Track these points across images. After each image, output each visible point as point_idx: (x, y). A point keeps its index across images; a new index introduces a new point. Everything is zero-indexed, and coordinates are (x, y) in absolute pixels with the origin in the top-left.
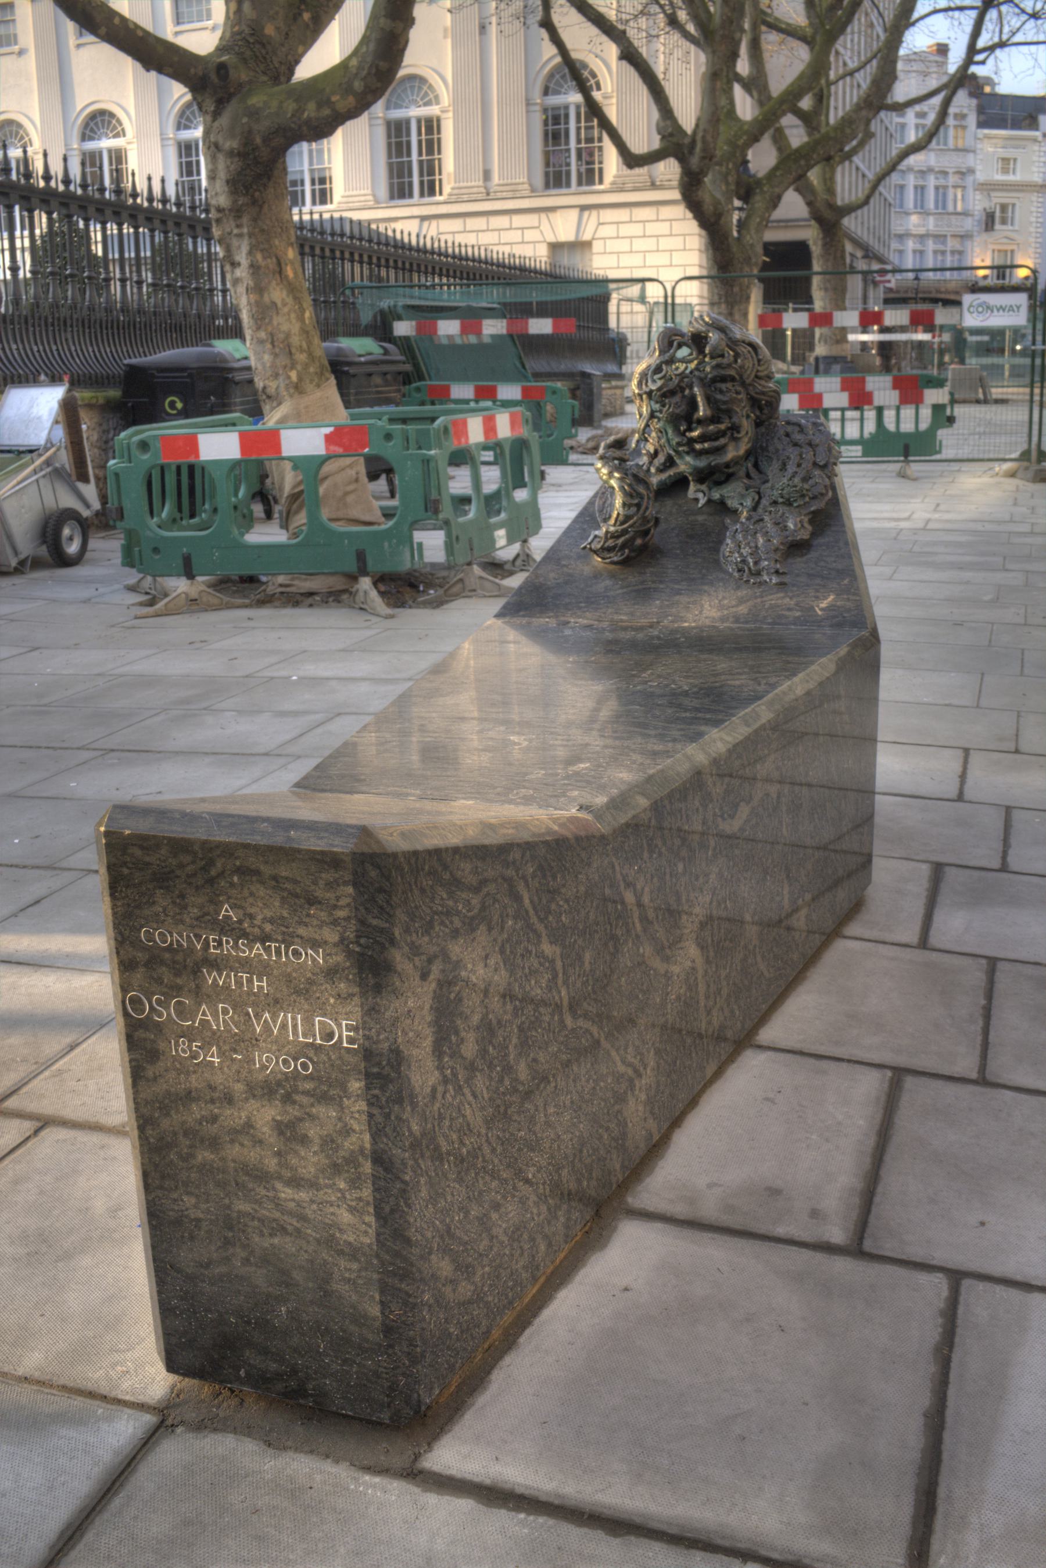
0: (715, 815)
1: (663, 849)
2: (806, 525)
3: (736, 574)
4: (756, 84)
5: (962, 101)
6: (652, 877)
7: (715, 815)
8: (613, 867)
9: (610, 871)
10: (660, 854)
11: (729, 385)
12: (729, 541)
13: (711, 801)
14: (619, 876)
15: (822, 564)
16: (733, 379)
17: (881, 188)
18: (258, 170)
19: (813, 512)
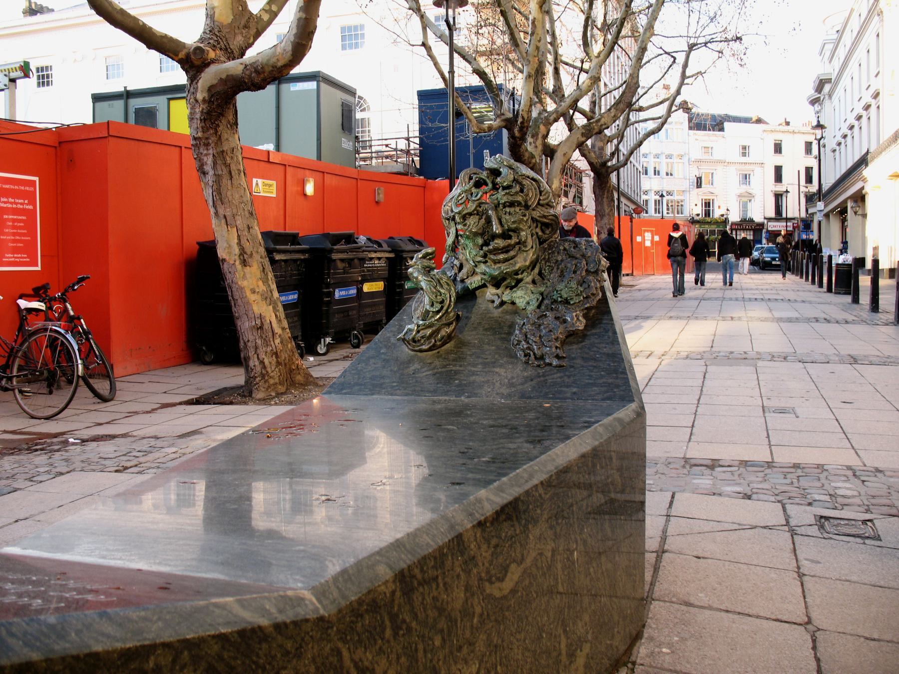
0: (481, 579)
1: (414, 624)
2: (581, 318)
3: (524, 359)
4: (557, 94)
5: (680, 117)
6: (398, 658)
7: (481, 579)
8: (339, 653)
9: (334, 660)
10: (409, 630)
11: (517, 209)
12: (517, 332)
13: (476, 565)
14: (347, 663)
15: (595, 349)
16: (519, 204)
17: (631, 159)
18: (218, 109)
19: (586, 308)
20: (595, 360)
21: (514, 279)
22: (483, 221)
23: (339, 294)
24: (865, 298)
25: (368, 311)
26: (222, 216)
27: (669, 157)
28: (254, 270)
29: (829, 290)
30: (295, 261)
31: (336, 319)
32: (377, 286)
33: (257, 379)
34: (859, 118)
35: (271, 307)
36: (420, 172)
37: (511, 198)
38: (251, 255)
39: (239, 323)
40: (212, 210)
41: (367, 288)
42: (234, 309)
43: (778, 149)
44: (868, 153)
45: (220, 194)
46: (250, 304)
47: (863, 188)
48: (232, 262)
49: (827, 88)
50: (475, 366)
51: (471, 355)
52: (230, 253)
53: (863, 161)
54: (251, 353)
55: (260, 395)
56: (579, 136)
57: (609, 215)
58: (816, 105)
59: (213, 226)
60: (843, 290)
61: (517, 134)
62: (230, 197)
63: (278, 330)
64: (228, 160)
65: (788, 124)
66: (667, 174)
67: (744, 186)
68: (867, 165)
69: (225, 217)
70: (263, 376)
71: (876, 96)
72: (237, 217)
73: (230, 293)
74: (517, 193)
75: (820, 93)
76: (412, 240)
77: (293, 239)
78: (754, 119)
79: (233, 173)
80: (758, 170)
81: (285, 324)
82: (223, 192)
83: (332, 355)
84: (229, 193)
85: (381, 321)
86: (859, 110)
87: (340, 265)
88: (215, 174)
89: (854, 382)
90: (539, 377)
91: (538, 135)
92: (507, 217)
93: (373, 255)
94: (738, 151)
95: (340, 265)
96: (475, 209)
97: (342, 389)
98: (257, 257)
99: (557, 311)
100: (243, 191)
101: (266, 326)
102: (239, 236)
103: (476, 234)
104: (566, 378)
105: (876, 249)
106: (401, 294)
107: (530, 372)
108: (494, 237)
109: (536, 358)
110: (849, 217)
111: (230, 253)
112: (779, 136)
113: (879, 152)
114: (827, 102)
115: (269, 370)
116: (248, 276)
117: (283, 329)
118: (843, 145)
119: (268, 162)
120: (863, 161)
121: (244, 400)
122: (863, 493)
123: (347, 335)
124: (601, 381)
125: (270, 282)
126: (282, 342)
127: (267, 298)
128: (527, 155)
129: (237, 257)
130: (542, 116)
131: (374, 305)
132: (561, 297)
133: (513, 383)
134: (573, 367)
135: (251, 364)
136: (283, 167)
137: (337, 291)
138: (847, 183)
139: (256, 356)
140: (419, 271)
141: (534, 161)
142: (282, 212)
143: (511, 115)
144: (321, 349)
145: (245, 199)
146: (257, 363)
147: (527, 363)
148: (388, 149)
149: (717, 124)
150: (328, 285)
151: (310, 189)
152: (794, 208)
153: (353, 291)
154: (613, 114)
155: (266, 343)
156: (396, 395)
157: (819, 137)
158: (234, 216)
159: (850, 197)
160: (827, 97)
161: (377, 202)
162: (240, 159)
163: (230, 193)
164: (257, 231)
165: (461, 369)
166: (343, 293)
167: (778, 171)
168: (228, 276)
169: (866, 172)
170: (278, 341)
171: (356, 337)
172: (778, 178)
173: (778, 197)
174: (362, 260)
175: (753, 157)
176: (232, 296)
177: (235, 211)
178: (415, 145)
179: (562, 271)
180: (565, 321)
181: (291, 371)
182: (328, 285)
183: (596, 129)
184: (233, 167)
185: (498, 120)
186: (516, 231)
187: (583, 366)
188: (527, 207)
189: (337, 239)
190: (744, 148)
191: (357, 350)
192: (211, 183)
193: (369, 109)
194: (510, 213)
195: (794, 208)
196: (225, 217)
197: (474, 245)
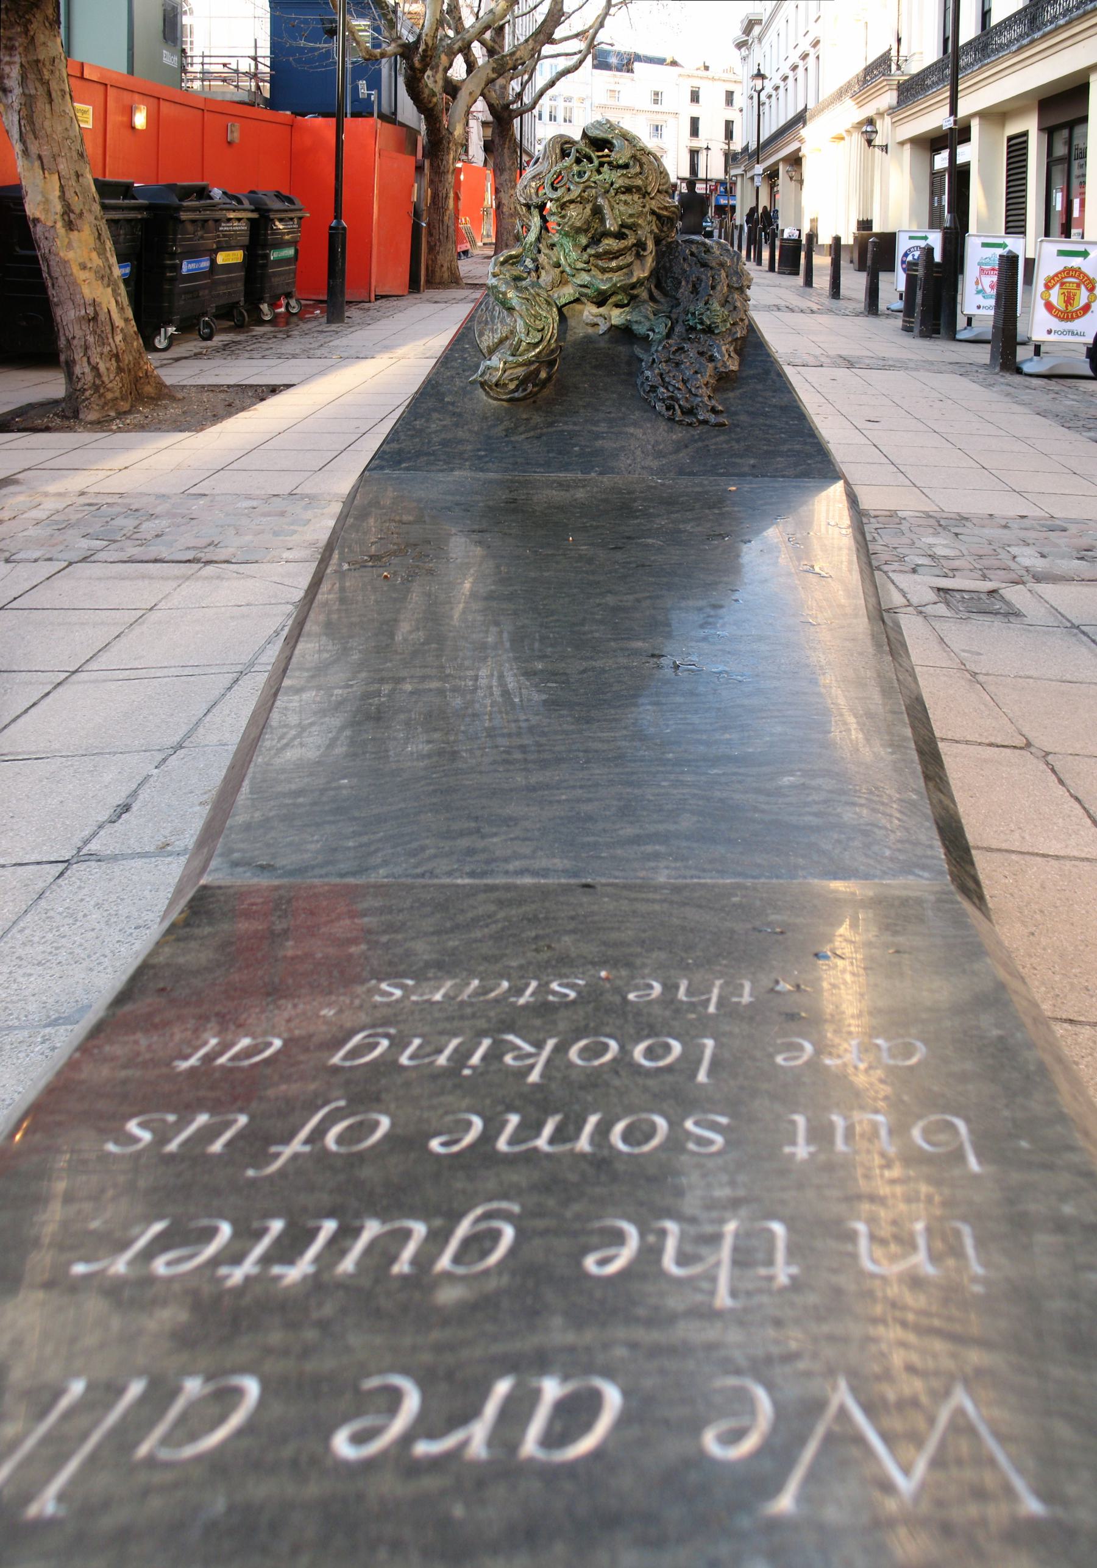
11: (636, 197)
15: (760, 399)
20: (765, 415)
21: (629, 294)
22: (588, 211)
23: (187, 267)
24: (822, 281)
25: (222, 290)
26: (35, 157)
27: (568, 99)
28: (85, 236)
29: (772, 269)
30: (129, 221)
31: (180, 302)
32: (235, 257)
33: (88, 393)
34: (795, 68)
35: (109, 290)
36: (272, 104)
37: (628, 182)
38: (81, 214)
39: (59, 312)
40: (18, 147)
41: (222, 258)
42: (51, 291)
43: (695, 97)
44: (805, 109)
45: (32, 123)
46: (78, 285)
47: (799, 149)
48: (50, 224)
49: (757, 30)
50: (596, 423)
51: (584, 407)
52: (47, 211)
53: (800, 119)
54: (78, 355)
55: (92, 416)
56: (490, 71)
57: (510, 169)
58: (743, 50)
59: (19, 170)
60: (787, 270)
61: (417, 64)
62: (49, 130)
63: (119, 322)
64: (47, 75)
65: (707, 68)
66: (565, 121)
67: (655, 140)
68: (805, 124)
69: (40, 157)
70: (96, 388)
71: (816, 44)
72: (60, 160)
73: (44, 268)
74: (637, 175)
75: (748, 35)
76: (279, 196)
77: (126, 190)
78: (668, 61)
79: (54, 95)
80: (671, 120)
81: (129, 313)
82: (38, 121)
83: (177, 351)
84: (47, 124)
85: (238, 303)
86: (794, 58)
87: (190, 227)
88: (24, 94)
89: (866, 393)
90: (696, 441)
91: (438, 67)
92: (622, 208)
93: (232, 215)
94: (649, 97)
95: (190, 227)
96: (580, 196)
97: (400, 462)
98: (89, 218)
99: (699, 343)
100: (68, 122)
101: (103, 317)
102: (62, 187)
103: (579, 231)
104: (734, 444)
105: (814, 221)
106: (264, 266)
107: (679, 434)
108: (606, 234)
109: (683, 413)
110: (780, 181)
111: (47, 211)
112: (696, 83)
113: (822, 108)
114: (756, 46)
115: (105, 379)
116: (75, 245)
117: (126, 320)
118: (774, 98)
119: (82, 77)
120: (800, 119)
121: (66, 423)
122: (965, 552)
123: (195, 321)
124: (785, 448)
125: (109, 255)
126: (124, 339)
127: (104, 277)
128: (427, 92)
129: (58, 217)
130: (444, 43)
131: (230, 281)
132: (702, 323)
133: (660, 452)
134: (737, 426)
135: (78, 370)
136: (156, 101)
137: (185, 263)
138: (780, 142)
139: (85, 359)
140: (507, 283)
141: (435, 100)
142: (100, 151)
143: (412, 39)
144: (160, 342)
145: (71, 134)
146: (87, 370)
147: (671, 419)
148: (226, 70)
149: (627, 64)
150: (173, 255)
151: (140, 120)
152: (713, 167)
153: (205, 264)
154: (531, 47)
155: (102, 341)
156: (488, 470)
157: (759, 88)
158: (54, 157)
159: (785, 160)
160: (756, 41)
161: (229, 143)
162: (65, 75)
163: (47, 123)
164: (89, 179)
165: (577, 428)
166: (193, 266)
167: (695, 123)
168: (43, 244)
169: (805, 132)
170: (119, 338)
171: (207, 325)
172: (695, 132)
173: (694, 153)
174: (217, 221)
175: (667, 104)
176: (49, 273)
177: (56, 150)
178: (265, 69)
179: (694, 286)
180: (712, 359)
181: (137, 379)
182: (173, 255)
183: (511, 63)
184: (54, 86)
185: (393, 45)
186: (633, 227)
187: (752, 426)
188: (645, 194)
189: (186, 193)
190: (656, 94)
191: (209, 343)
192: (16, 106)
193: (191, 13)
194: (626, 203)
195: (713, 167)
196: (40, 157)
197: (574, 246)
